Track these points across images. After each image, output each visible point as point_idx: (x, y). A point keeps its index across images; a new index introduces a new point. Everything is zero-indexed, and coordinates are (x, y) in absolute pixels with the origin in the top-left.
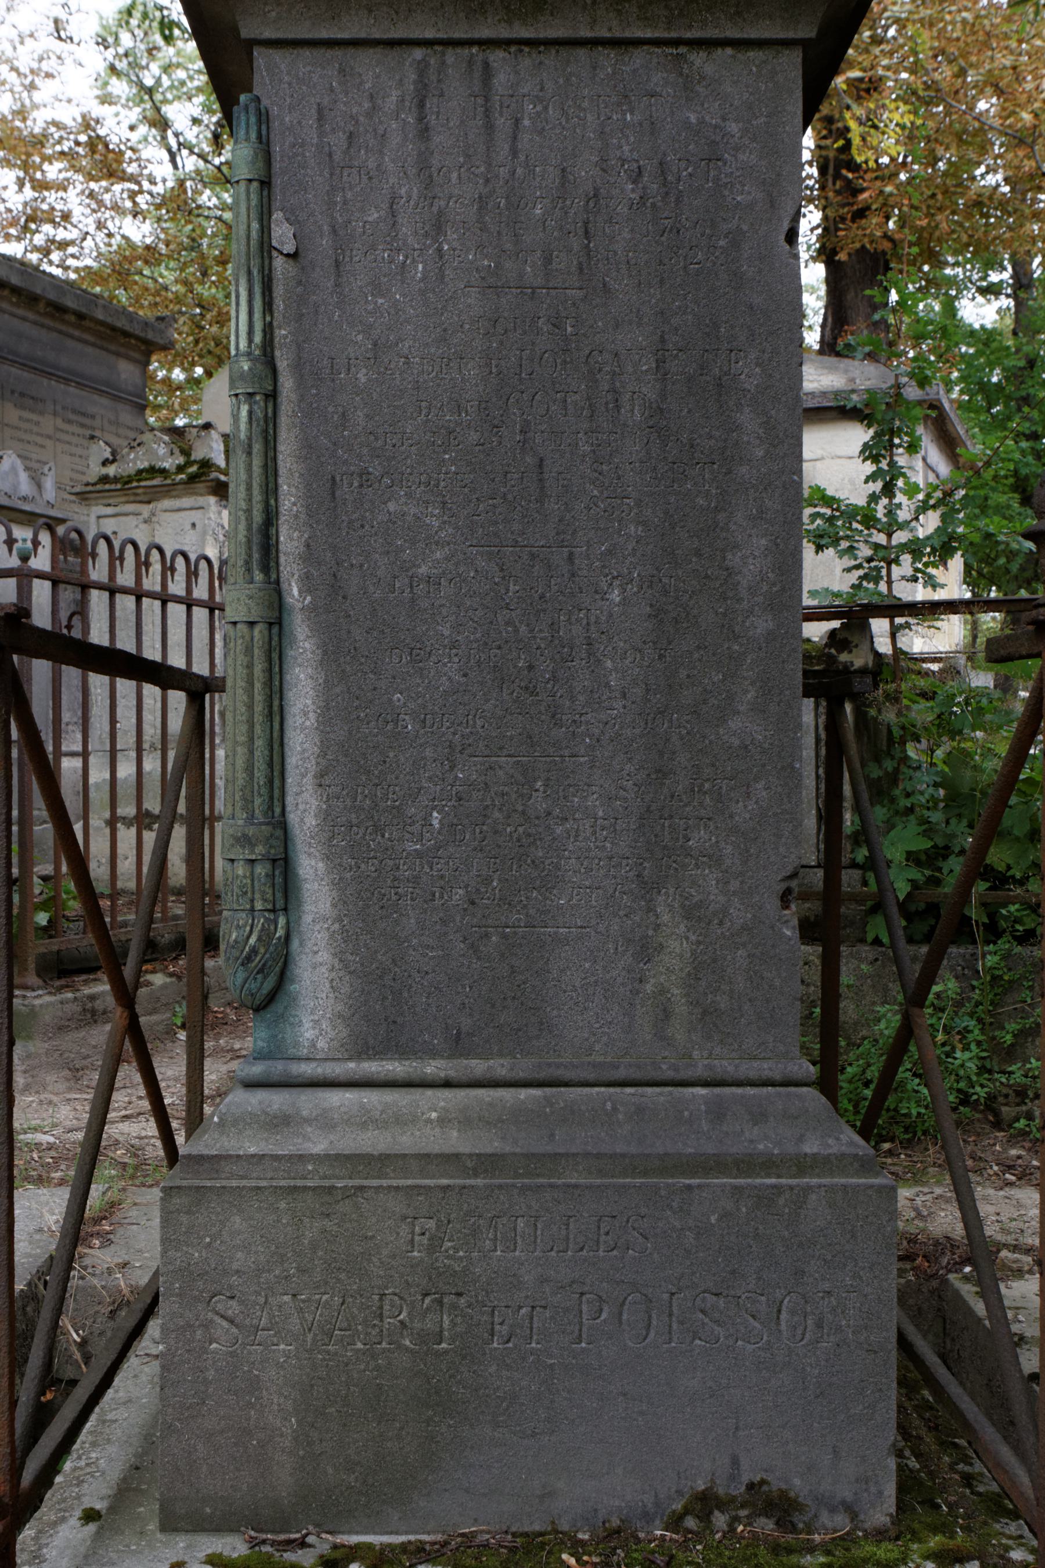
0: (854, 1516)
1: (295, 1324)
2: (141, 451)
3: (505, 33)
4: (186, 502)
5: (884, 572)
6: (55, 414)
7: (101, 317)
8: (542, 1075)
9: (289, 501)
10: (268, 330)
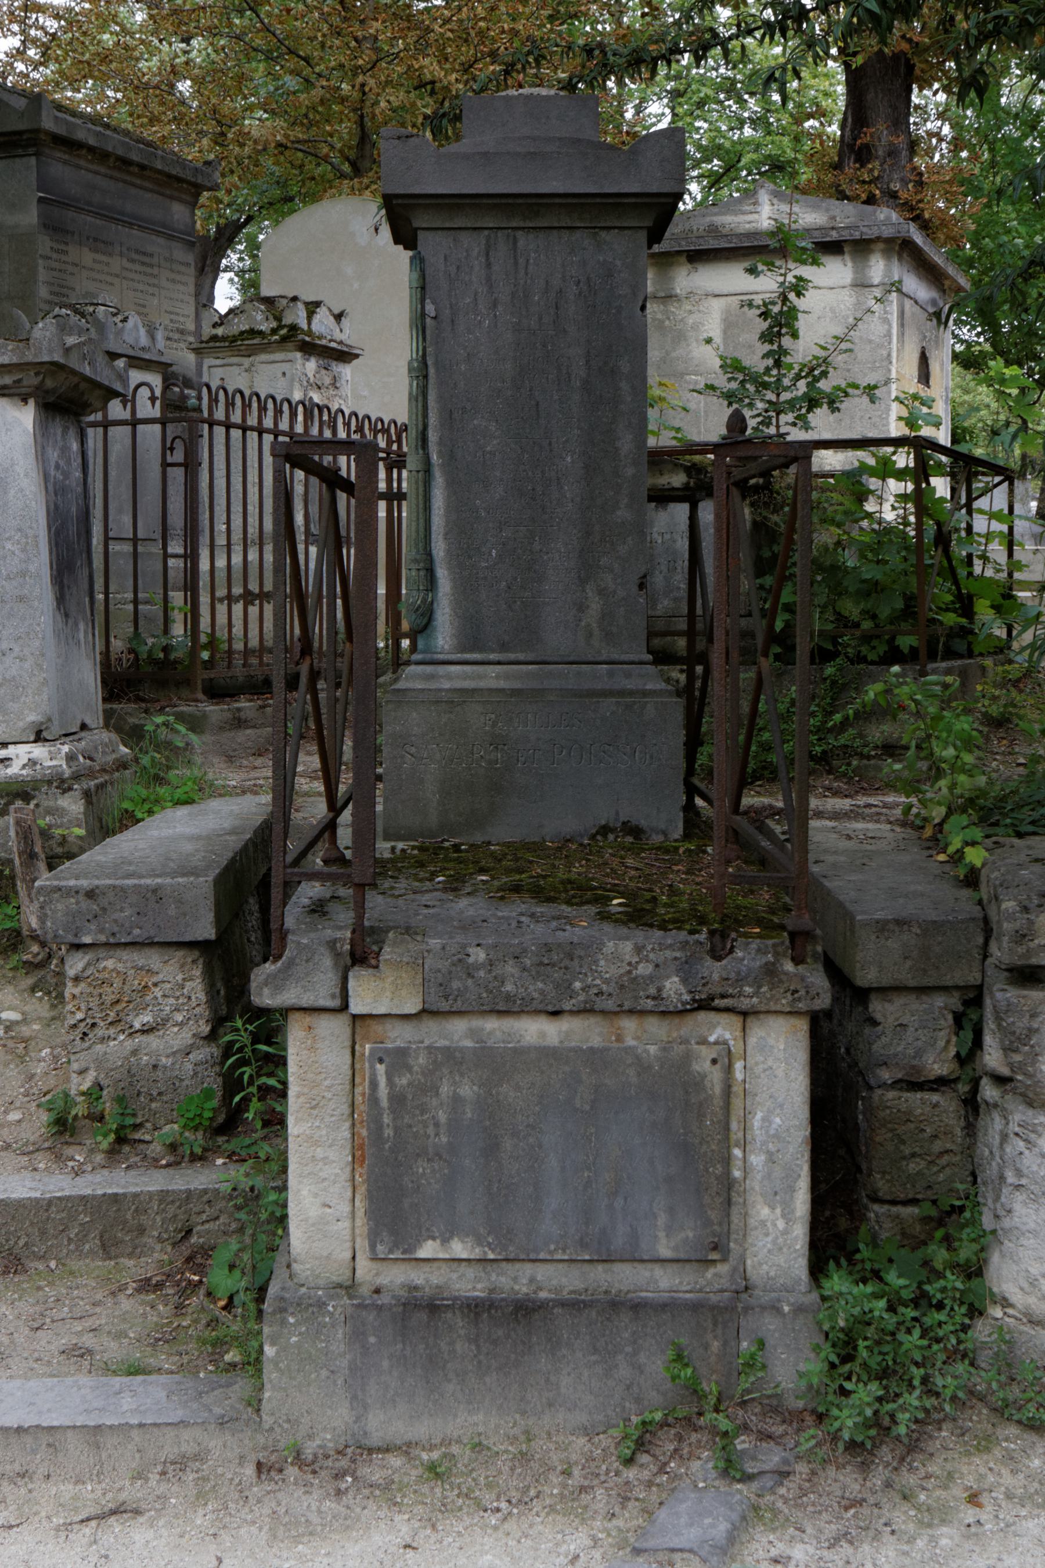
0: (666, 835)
1: (438, 756)
2: (243, 317)
3: (522, 224)
4: (278, 356)
5: (774, 421)
6: (121, 255)
7: (159, 167)
8: (539, 659)
9: (433, 419)
10: (424, 349)
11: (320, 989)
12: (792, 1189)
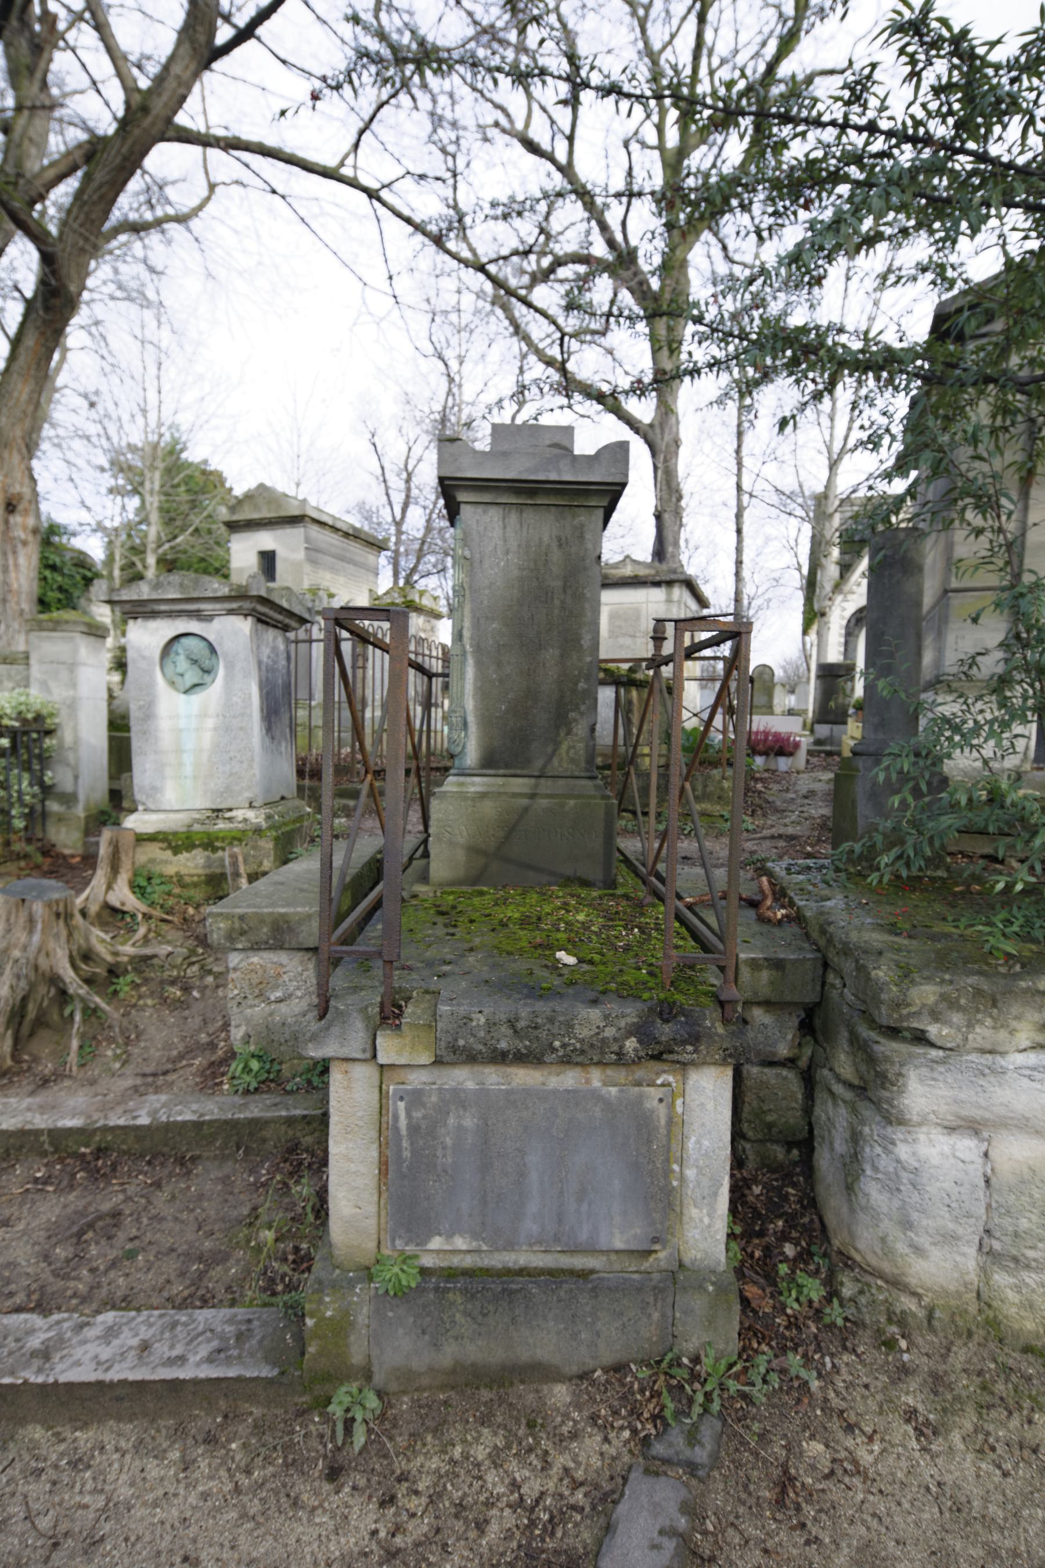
11: (355, 1041)
12: (715, 1194)
